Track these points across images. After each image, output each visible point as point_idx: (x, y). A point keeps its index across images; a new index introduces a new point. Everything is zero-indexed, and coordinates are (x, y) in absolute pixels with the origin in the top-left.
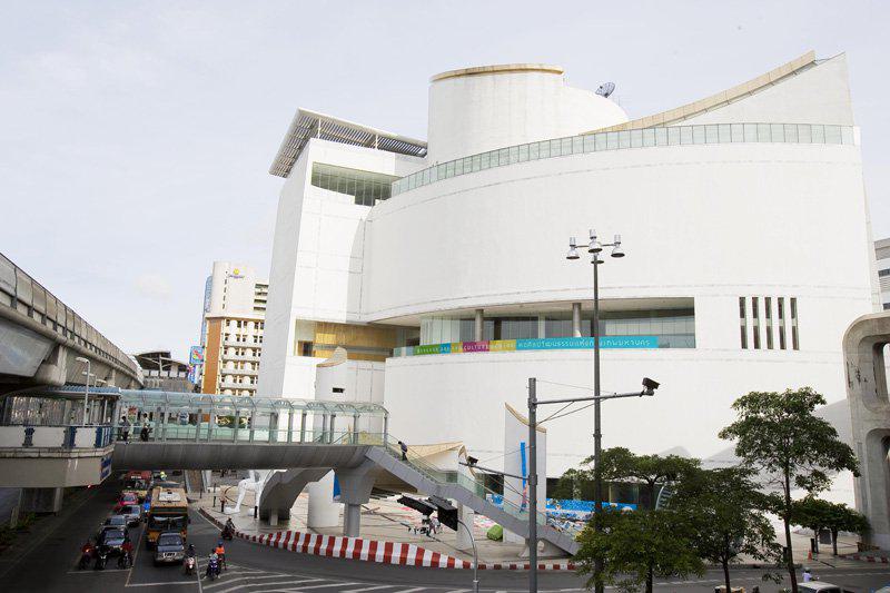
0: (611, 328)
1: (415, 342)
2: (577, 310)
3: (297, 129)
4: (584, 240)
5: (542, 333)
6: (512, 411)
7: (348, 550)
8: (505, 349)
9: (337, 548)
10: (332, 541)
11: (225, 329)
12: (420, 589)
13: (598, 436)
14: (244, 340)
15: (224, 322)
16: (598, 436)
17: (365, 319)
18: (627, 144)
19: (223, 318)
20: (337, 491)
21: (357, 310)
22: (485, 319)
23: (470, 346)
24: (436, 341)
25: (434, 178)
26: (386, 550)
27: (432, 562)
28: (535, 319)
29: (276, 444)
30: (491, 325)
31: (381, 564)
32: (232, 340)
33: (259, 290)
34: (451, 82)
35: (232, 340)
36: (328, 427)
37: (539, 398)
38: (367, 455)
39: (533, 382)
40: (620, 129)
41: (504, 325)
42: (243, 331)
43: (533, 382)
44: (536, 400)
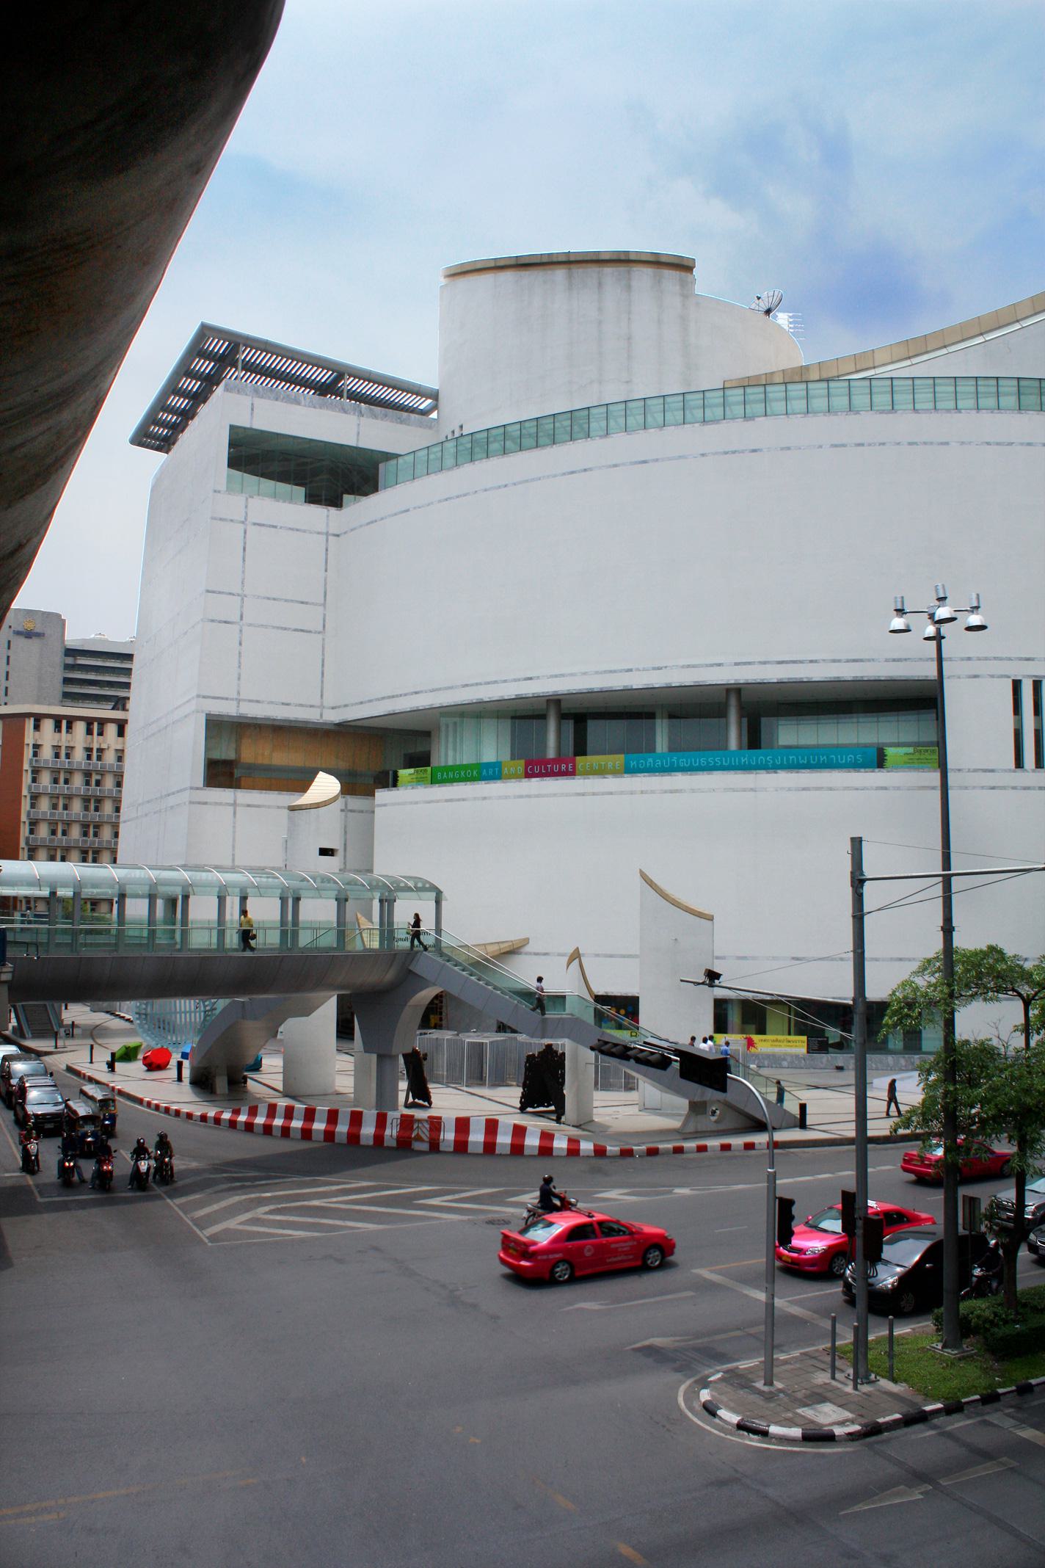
0: (789, 733)
1: (420, 760)
2: (733, 701)
3: (197, 349)
4: (920, 599)
5: (661, 742)
6: (651, 883)
7: (388, 1132)
8: (601, 772)
9: (368, 1130)
10: (356, 1118)
11: (30, 736)
12: (501, 1189)
13: (948, 929)
14: (68, 756)
15: (30, 723)
16: (948, 929)
17: (333, 717)
18: (801, 405)
19: (29, 715)
20: (344, 1031)
21: (317, 701)
22: (563, 716)
23: (537, 768)
24: (467, 757)
25: (449, 461)
26: (457, 1131)
27: (513, 1146)
28: (651, 716)
29: (189, 955)
30: (569, 726)
31: (367, 1147)
32: (47, 753)
33: (70, 660)
34: (488, 278)
35: (47, 753)
36: (290, 918)
37: (868, 871)
38: (411, 968)
39: (857, 844)
40: (799, 376)
41: (592, 726)
42: (96, 742)
43: (857, 844)
44: (862, 874)
